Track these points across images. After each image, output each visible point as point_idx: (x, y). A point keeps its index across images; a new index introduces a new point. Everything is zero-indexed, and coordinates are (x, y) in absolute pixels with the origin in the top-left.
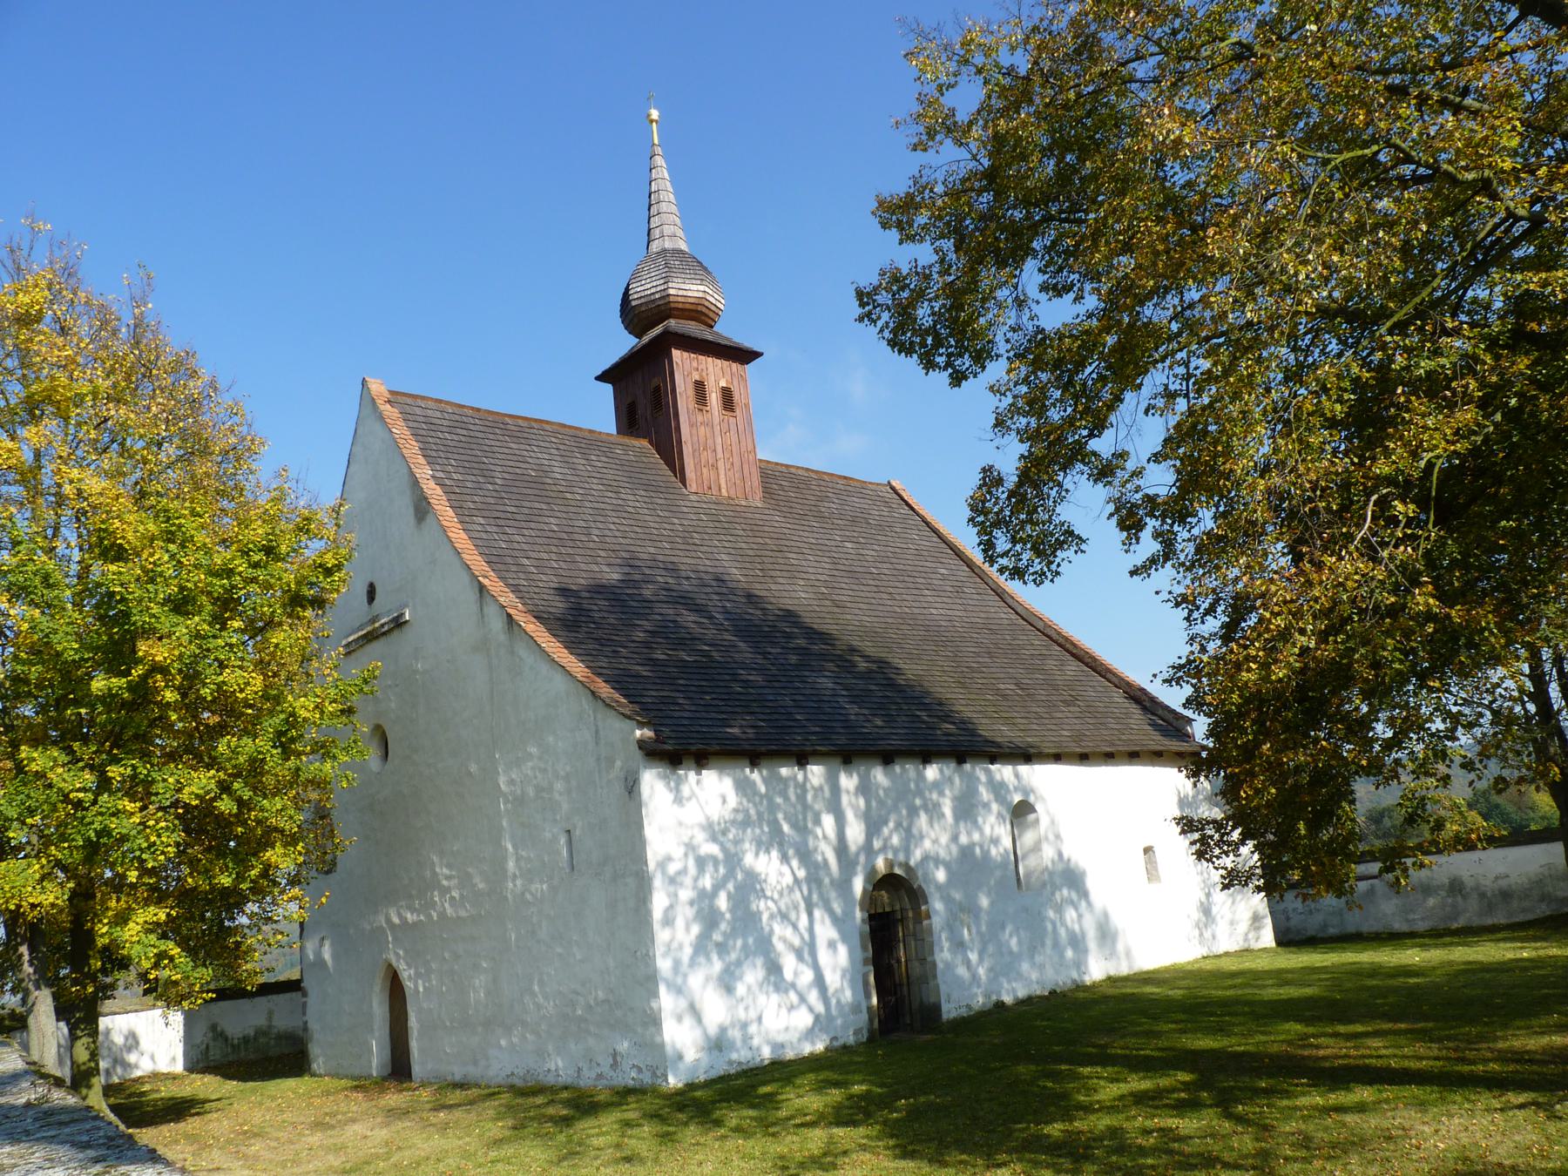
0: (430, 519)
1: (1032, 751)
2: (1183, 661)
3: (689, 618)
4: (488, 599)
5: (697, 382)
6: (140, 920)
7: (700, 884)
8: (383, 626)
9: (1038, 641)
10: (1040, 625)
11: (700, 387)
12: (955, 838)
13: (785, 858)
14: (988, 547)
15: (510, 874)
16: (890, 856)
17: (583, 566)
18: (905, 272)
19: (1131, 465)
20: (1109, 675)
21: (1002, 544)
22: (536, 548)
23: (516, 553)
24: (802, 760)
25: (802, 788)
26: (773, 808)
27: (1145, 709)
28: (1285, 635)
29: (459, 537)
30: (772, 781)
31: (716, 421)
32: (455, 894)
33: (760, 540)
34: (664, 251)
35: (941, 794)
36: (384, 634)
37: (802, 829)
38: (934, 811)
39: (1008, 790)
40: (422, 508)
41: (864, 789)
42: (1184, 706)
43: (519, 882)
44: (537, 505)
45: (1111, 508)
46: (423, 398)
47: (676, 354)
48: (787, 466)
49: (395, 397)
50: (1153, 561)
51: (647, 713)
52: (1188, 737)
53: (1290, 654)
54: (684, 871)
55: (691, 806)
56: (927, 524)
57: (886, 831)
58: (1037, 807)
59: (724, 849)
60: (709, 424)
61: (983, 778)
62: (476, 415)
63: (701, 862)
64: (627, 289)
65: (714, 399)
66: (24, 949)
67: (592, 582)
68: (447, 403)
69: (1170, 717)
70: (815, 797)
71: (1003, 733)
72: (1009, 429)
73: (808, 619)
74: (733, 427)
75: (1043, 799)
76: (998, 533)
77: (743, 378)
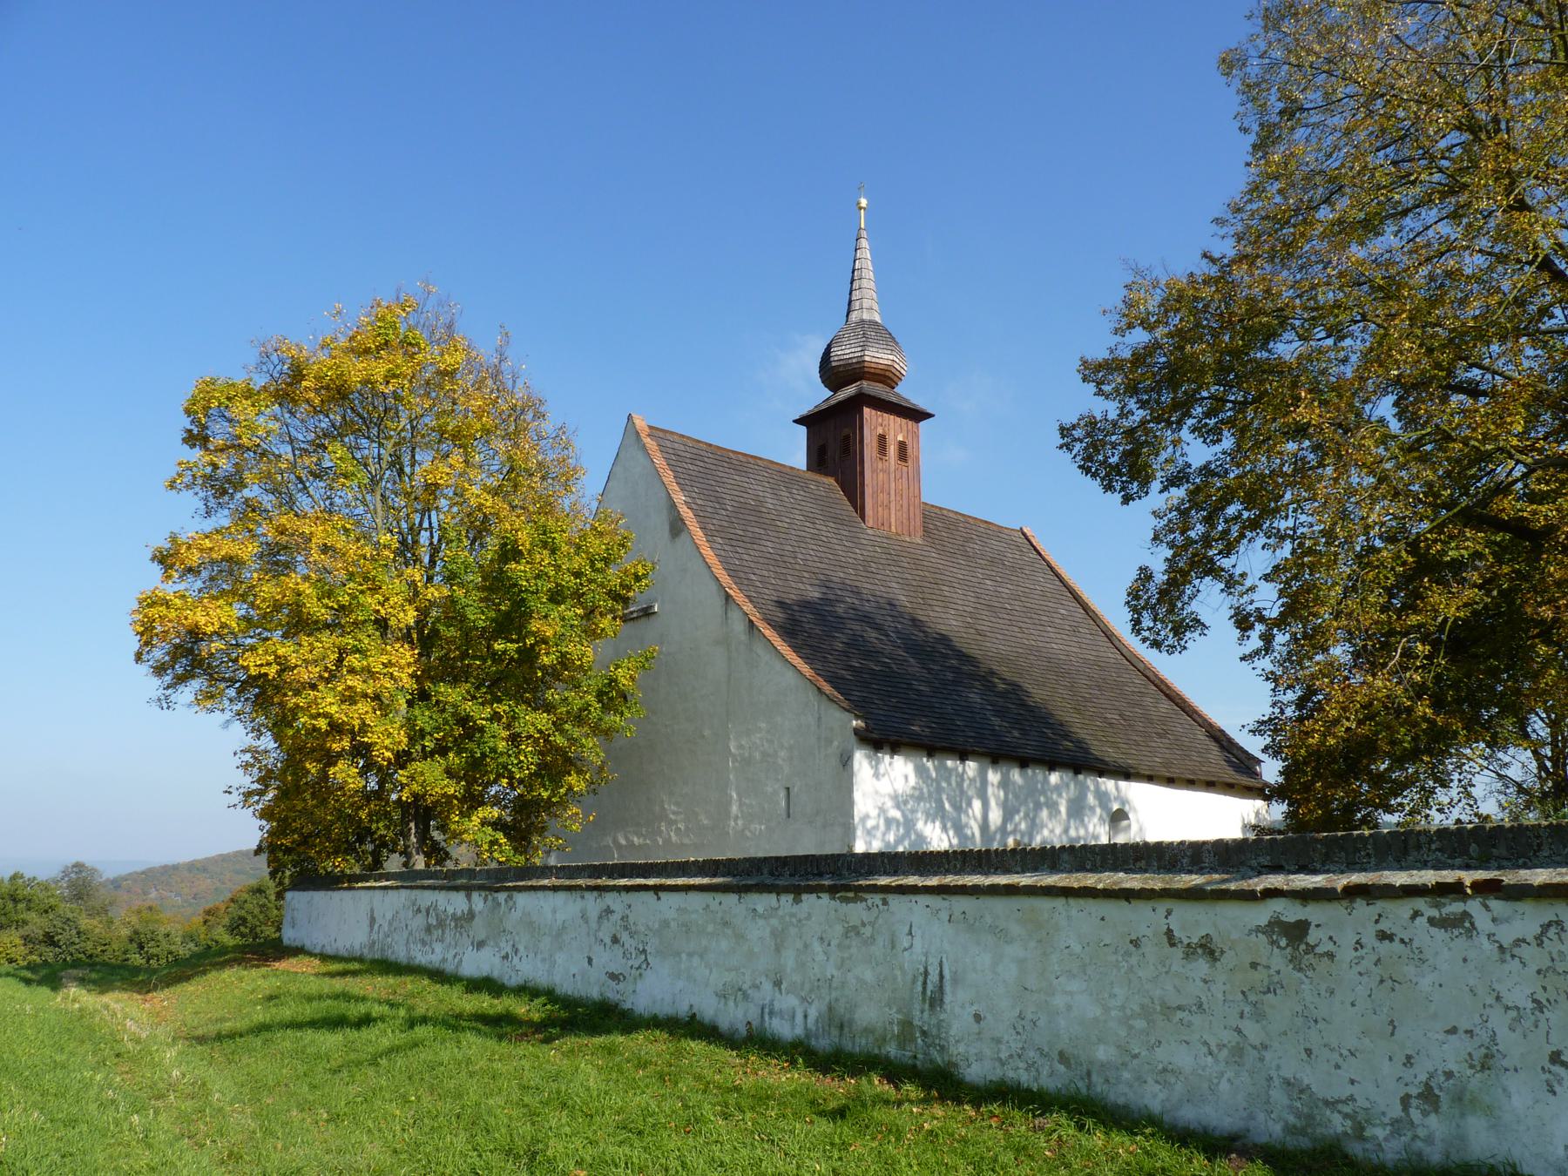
0: (684, 536)
1: (1132, 771)
2: (1266, 718)
3: (872, 635)
4: (734, 606)
5: (900, 442)
6: (480, 815)
7: (887, 838)
8: (632, 613)
9: (1139, 680)
10: (1141, 666)
11: (882, 440)
12: (1066, 831)
13: (944, 829)
14: (1136, 623)
15: (732, 815)
16: (1018, 838)
17: (793, 584)
18: (1098, 418)
19: (1248, 583)
20: (1195, 716)
21: (1147, 622)
22: (760, 566)
23: (747, 570)
24: (963, 756)
25: (961, 777)
26: (939, 790)
27: (1222, 747)
28: (1336, 722)
29: (708, 552)
30: (941, 768)
31: (892, 469)
32: (681, 826)
33: (921, 573)
34: (863, 321)
35: (1060, 795)
36: (633, 619)
37: (958, 808)
38: (1053, 807)
39: (1109, 800)
40: (677, 527)
41: (1005, 784)
42: (1263, 751)
43: (740, 822)
44: (757, 530)
45: (1232, 612)
46: (672, 433)
47: (866, 410)
48: (941, 509)
49: (654, 431)
50: (1257, 653)
51: (857, 706)
52: (1256, 775)
53: (1340, 731)
54: (876, 827)
55: (885, 780)
56: (1052, 568)
57: (1017, 818)
58: (1131, 816)
59: (904, 815)
60: (886, 471)
61: (1092, 788)
62: (709, 449)
63: (889, 822)
64: (829, 348)
65: (892, 450)
66: (412, 825)
67: (799, 598)
68: (688, 438)
69: (1243, 757)
70: (970, 785)
71: (1110, 754)
72: (1162, 541)
73: (957, 643)
74: (905, 475)
75: (1135, 810)
76: (1145, 614)
77: (916, 435)
